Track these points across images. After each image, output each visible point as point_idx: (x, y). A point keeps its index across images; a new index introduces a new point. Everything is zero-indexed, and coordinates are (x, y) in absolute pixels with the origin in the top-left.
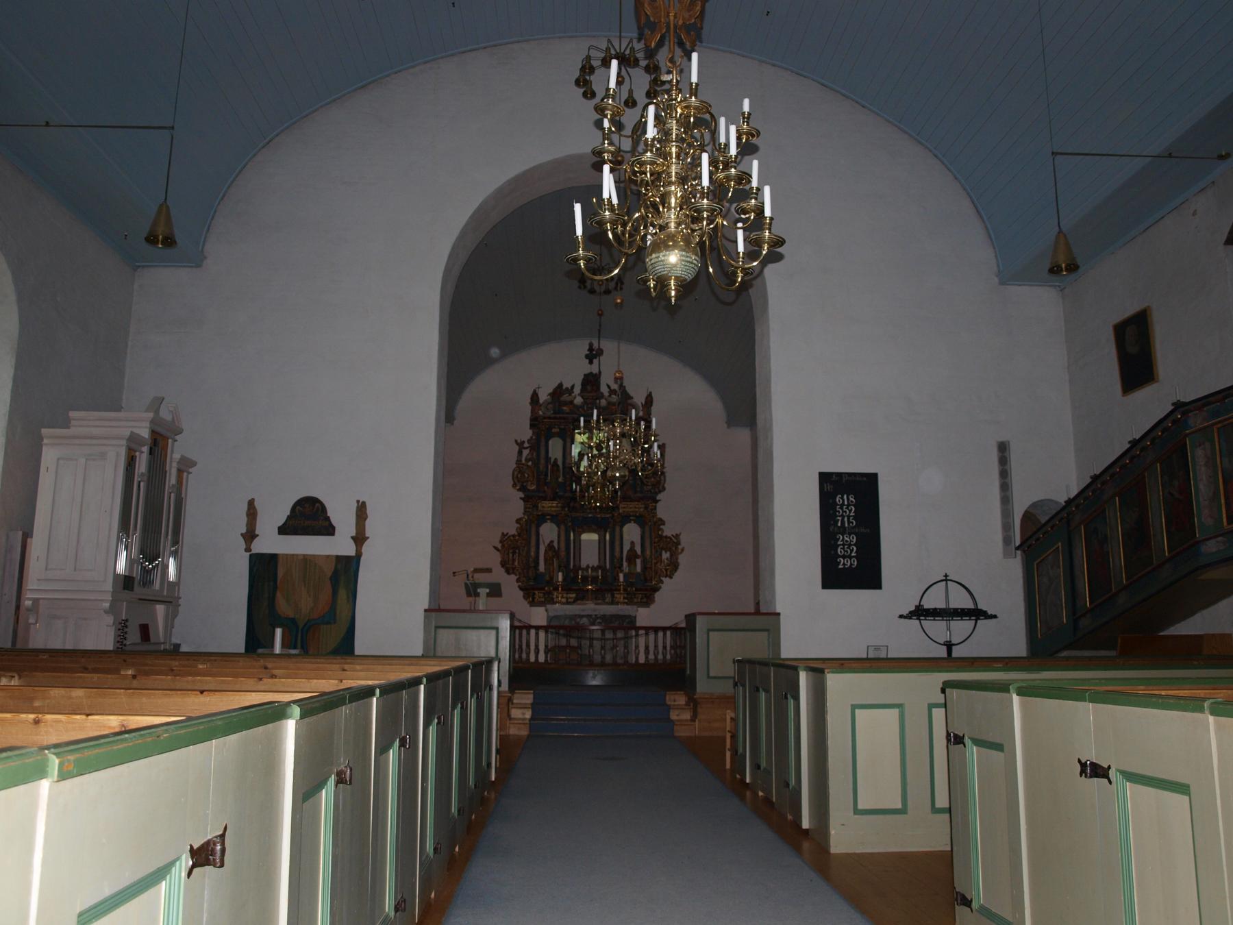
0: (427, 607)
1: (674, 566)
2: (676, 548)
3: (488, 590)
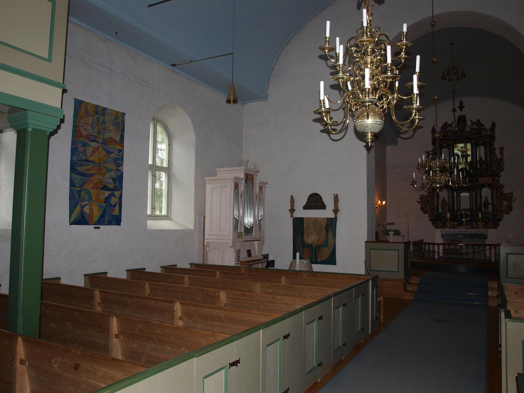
0: (366, 241)
1: (510, 209)
2: (511, 199)
3: (394, 233)
